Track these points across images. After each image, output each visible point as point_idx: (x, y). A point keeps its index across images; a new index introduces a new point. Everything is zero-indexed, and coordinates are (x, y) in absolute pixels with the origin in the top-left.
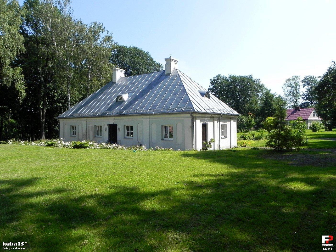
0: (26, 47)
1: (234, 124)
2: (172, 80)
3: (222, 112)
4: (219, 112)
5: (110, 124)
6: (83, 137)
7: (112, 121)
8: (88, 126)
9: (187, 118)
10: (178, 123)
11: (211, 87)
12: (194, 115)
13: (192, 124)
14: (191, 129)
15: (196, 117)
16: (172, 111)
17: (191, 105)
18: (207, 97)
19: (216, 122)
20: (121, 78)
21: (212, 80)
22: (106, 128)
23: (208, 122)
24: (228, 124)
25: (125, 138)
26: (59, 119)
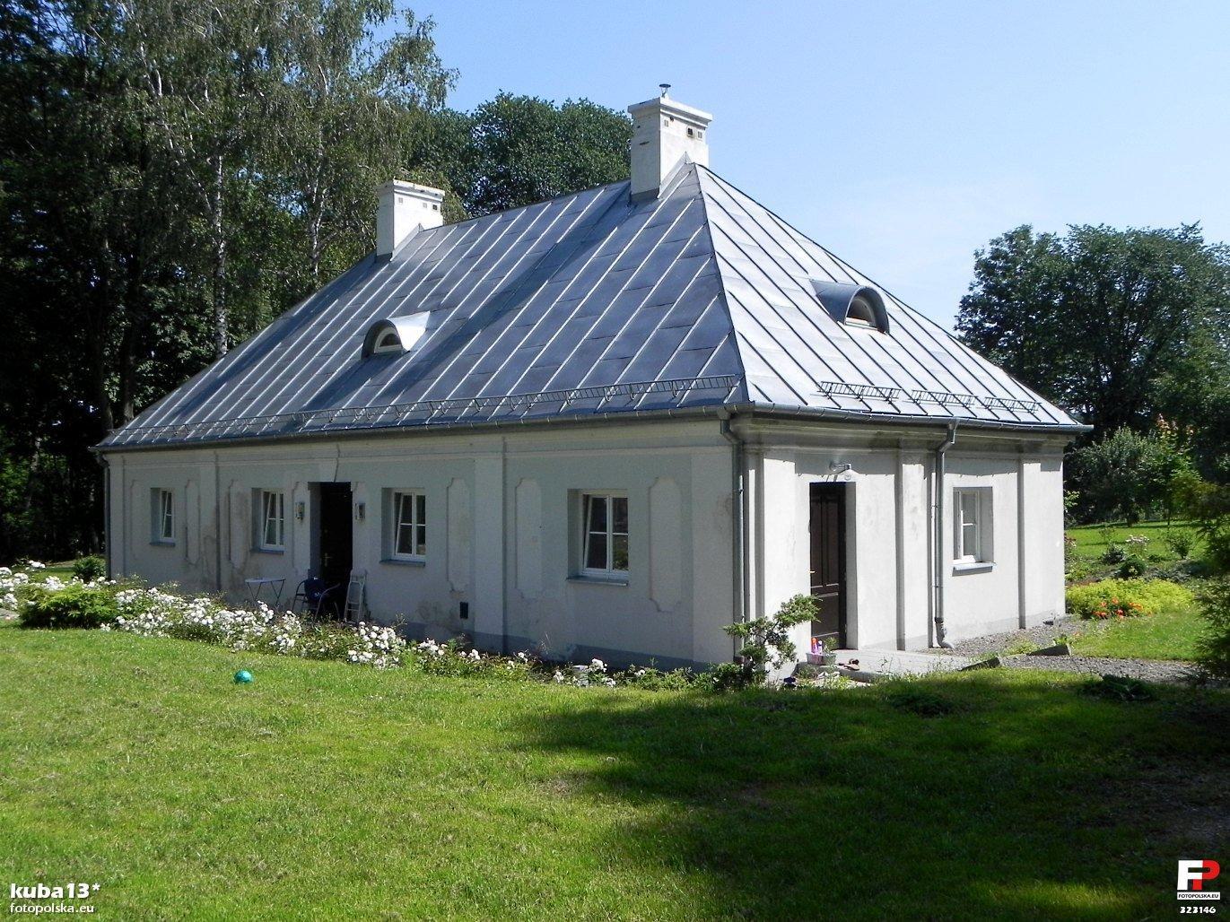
0: (980, 349)
1: (1045, 487)
2: (661, 223)
3: (959, 413)
4: (934, 411)
5: (322, 484)
6: (203, 549)
7: (326, 465)
8: (223, 492)
9: (705, 447)
10: (661, 478)
11: (979, 290)
12: (749, 431)
13: (736, 484)
14: (726, 520)
15: (760, 443)
16: (620, 402)
17: (736, 366)
18: (865, 322)
19: (914, 473)
20: (422, 232)
21: (987, 256)
22: (302, 504)
23: (850, 471)
24: (1001, 484)
25: (387, 561)
26: (105, 453)
